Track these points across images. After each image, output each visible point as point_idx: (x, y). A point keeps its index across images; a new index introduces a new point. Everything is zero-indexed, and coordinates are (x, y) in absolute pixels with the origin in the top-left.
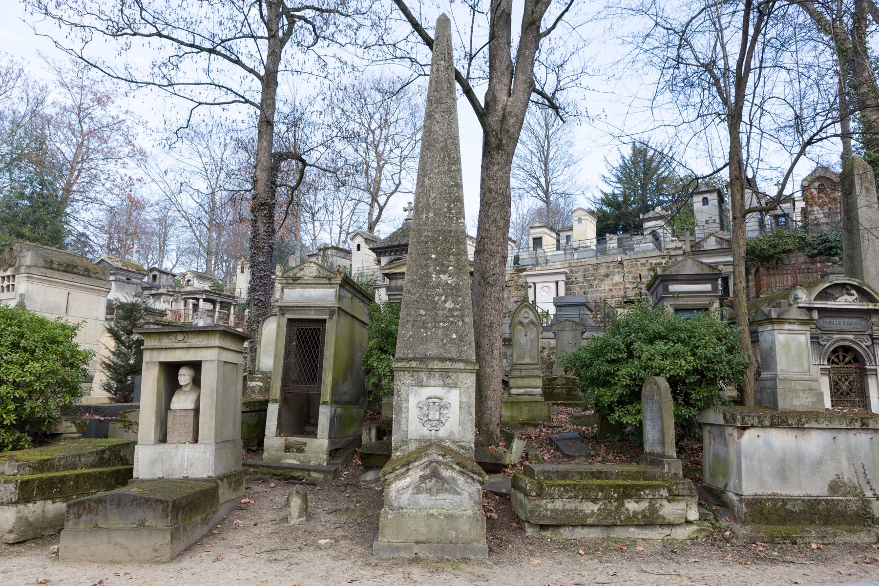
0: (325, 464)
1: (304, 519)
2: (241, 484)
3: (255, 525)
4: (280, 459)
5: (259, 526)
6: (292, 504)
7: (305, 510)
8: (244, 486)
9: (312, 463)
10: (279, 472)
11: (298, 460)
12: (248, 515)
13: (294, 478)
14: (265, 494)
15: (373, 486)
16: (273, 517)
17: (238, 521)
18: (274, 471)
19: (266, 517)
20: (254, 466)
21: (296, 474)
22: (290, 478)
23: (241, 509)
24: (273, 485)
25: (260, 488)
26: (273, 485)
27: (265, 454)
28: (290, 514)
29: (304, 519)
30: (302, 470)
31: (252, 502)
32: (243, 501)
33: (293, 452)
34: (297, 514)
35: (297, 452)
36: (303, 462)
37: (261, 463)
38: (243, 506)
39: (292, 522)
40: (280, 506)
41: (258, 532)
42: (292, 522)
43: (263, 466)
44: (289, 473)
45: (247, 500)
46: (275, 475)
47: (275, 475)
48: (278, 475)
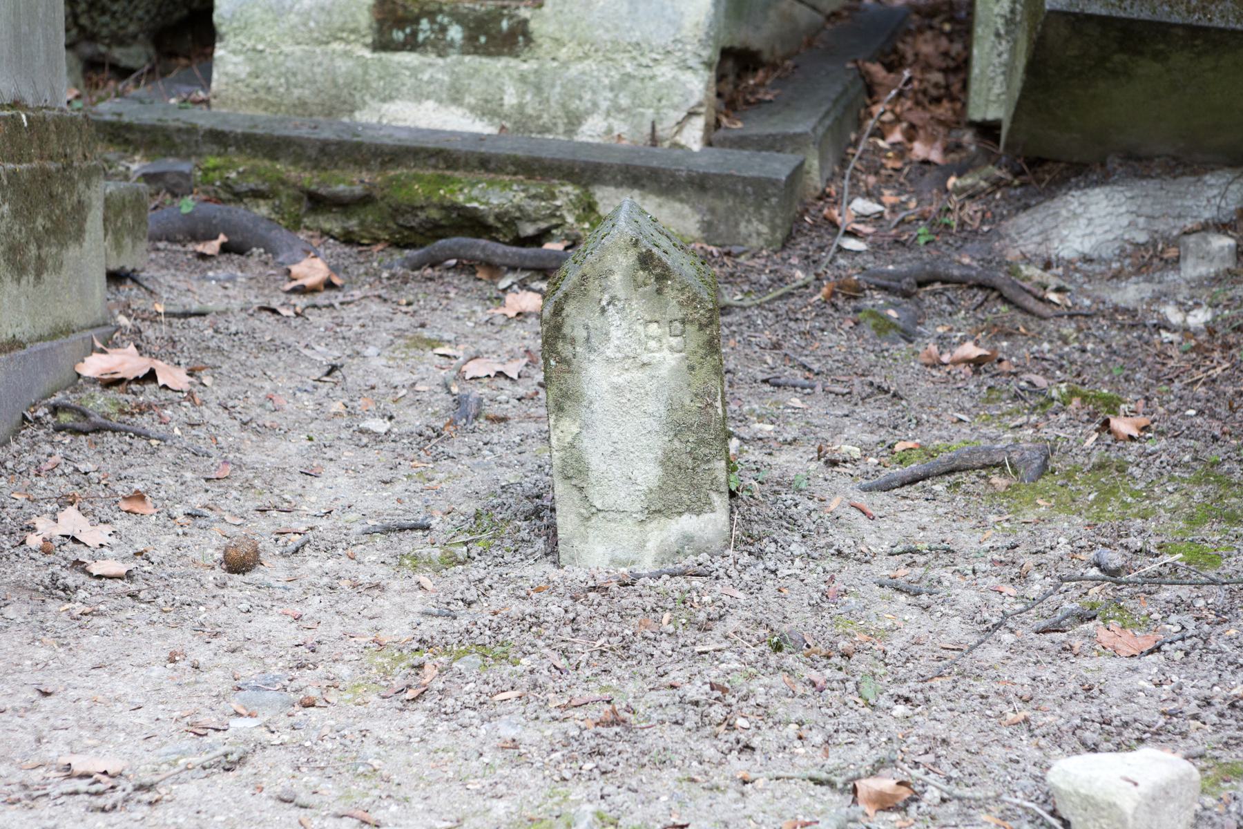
0: (693, 137)
1: (712, 522)
2: (67, 227)
3: (239, 564)
4: (341, 100)
5: (273, 570)
6: (598, 376)
7: (702, 450)
8: (93, 251)
9: (592, 130)
10: (349, 182)
11: (487, 109)
12: (147, 472)
13: (473, 224)
14: (266, 327)
15: (1131, 293)
16: (382, 503)
17: (71, 520)
18: (309, 179)
19: (316, 496)
20: (153, 139)
21: (491, 197)
22: (435, 231)
23: (89, 427)
24: (312, 270)
25: (224, 290)
26: (312, 270)
27: (228, 60)
28: (576, 470)
29: (712, 522)
30: (530, 168)
31: (172, 376)
32: (94, 366)
33: (441, 47)
34: (649, 474)
35: (471, 46)
36: (523, 121)
37: (202, 119)
38: (100, 403)
39: (595, 551)
40: (414, 420)
41: (275, 625)
42: (595, 551)
43: (219, 138)
44: (421, 189)
45: (126, 361)
46: (318, 202)
47: (318, 202)
48: (343, 205)
